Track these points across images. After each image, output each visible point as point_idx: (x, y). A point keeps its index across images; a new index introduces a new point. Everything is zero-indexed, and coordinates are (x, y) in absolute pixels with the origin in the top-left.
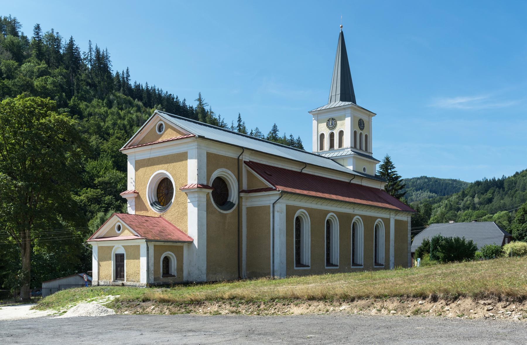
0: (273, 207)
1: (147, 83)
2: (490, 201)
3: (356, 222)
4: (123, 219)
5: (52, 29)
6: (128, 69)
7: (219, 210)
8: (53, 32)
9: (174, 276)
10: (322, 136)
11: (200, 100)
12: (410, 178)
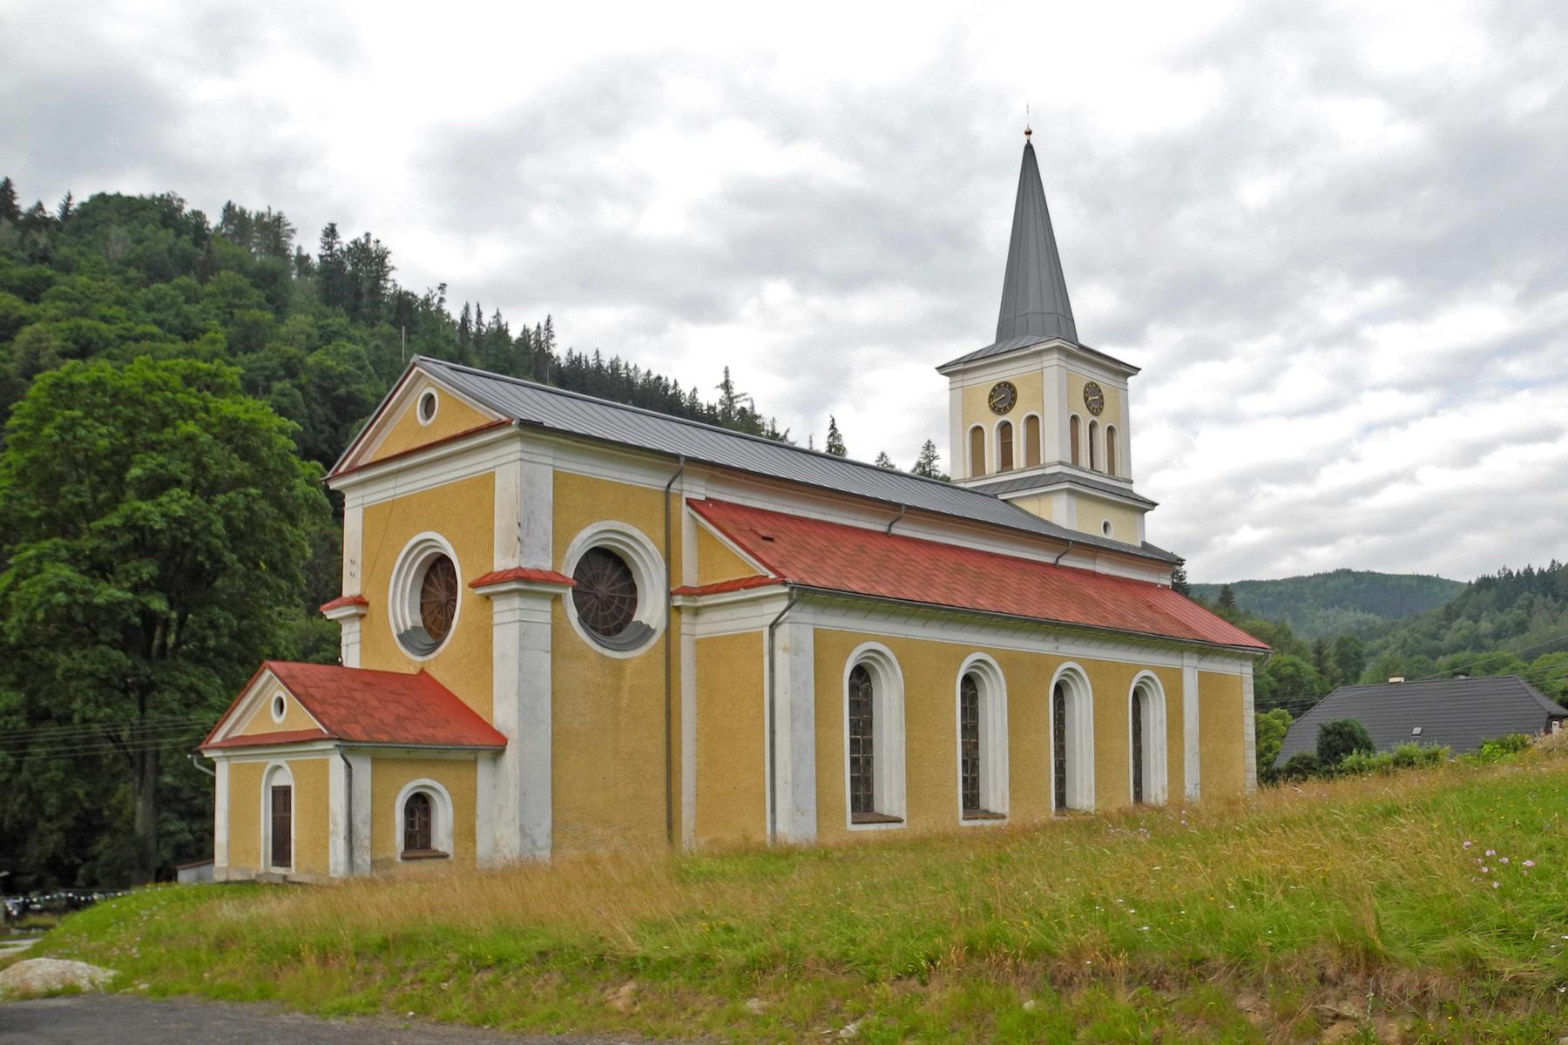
0: (772, 635)
1: (597, 352)
2: (1521, 627)
3: (1066, 679)
4: (287, 680)
5: (368, 235)
6: (549, 321)
7: (599, 649)
8: (368, 241)
9: (444, 856)
10: (977, 431)
11: (726, 386)
12: (1307, 575)
